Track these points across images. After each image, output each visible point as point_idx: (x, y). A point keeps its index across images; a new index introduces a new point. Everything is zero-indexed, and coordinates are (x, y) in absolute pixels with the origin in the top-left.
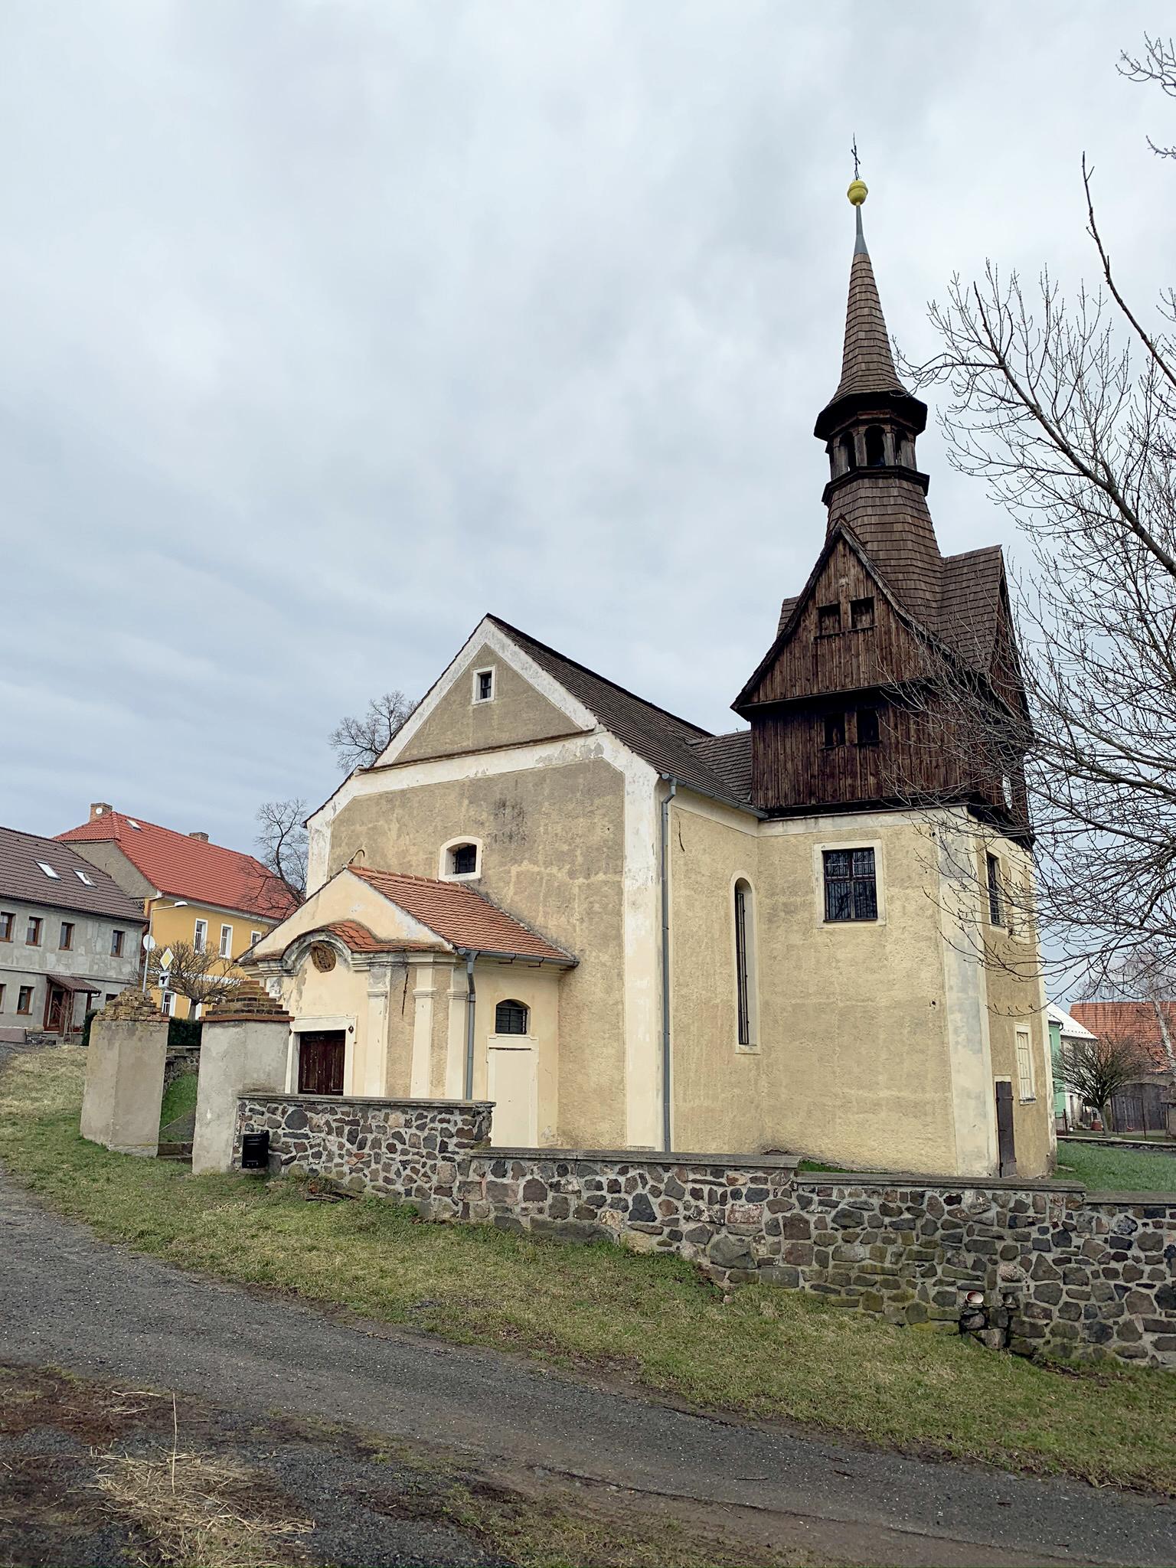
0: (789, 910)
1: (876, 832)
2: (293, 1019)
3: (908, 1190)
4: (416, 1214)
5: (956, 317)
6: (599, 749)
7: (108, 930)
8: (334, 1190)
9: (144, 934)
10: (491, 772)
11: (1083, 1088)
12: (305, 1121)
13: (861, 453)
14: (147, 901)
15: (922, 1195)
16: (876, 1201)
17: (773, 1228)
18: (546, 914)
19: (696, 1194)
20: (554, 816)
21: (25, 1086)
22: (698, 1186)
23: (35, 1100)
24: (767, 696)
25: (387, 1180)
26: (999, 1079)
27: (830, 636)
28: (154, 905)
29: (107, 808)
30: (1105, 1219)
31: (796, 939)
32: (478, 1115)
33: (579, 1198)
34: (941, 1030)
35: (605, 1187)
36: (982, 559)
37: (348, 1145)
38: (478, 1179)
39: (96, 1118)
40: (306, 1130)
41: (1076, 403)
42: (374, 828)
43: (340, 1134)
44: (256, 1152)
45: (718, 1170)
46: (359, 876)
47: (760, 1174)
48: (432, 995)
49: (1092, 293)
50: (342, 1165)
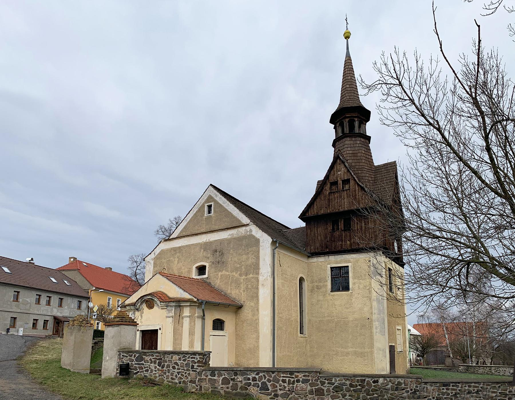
0: (318, 288)
1: (350, 260)
2: (138, 324)
3: (360, 378)
4: (183, 390)
5: (384, 67)
6: (251, 231)
7: (76, 300)
8: (153, 382)
9: (89, 302)
10: (212, 240)
11: (417, 351)
12: (142, 359)
13: (347, 129)
14: (90, 291)
15: (365, 380)
16: (348, 382)
17: (311, 392)
18: (231, 289)
19: (284, 381)
20: (235, 254)
21: (42, 351)
22: (284, 378)
23: (46, 355)
24: (310, 214)
25: (172, 379)
26: (390, 344)
27: (334, 192)
28: (92, 292)
29: (75, 259)
30: (429, 387)
31: (321, 298)
32: (205, 356)
33: (241, 383)
34: (371, 328)
35: (251, 379)
36: (389, 166)
37: (158, 367)
38: (205, 377)
39: (67, 359)
40: (143, 362)
41: (427, 99)
42: (169, 260)
43: (155, 363)
44: (125, 370)
45: (291, 373)
46: (163, 276)
47: (307, 374)
48: (189, 317)
49: (434, 58)
50: (156, 374)
